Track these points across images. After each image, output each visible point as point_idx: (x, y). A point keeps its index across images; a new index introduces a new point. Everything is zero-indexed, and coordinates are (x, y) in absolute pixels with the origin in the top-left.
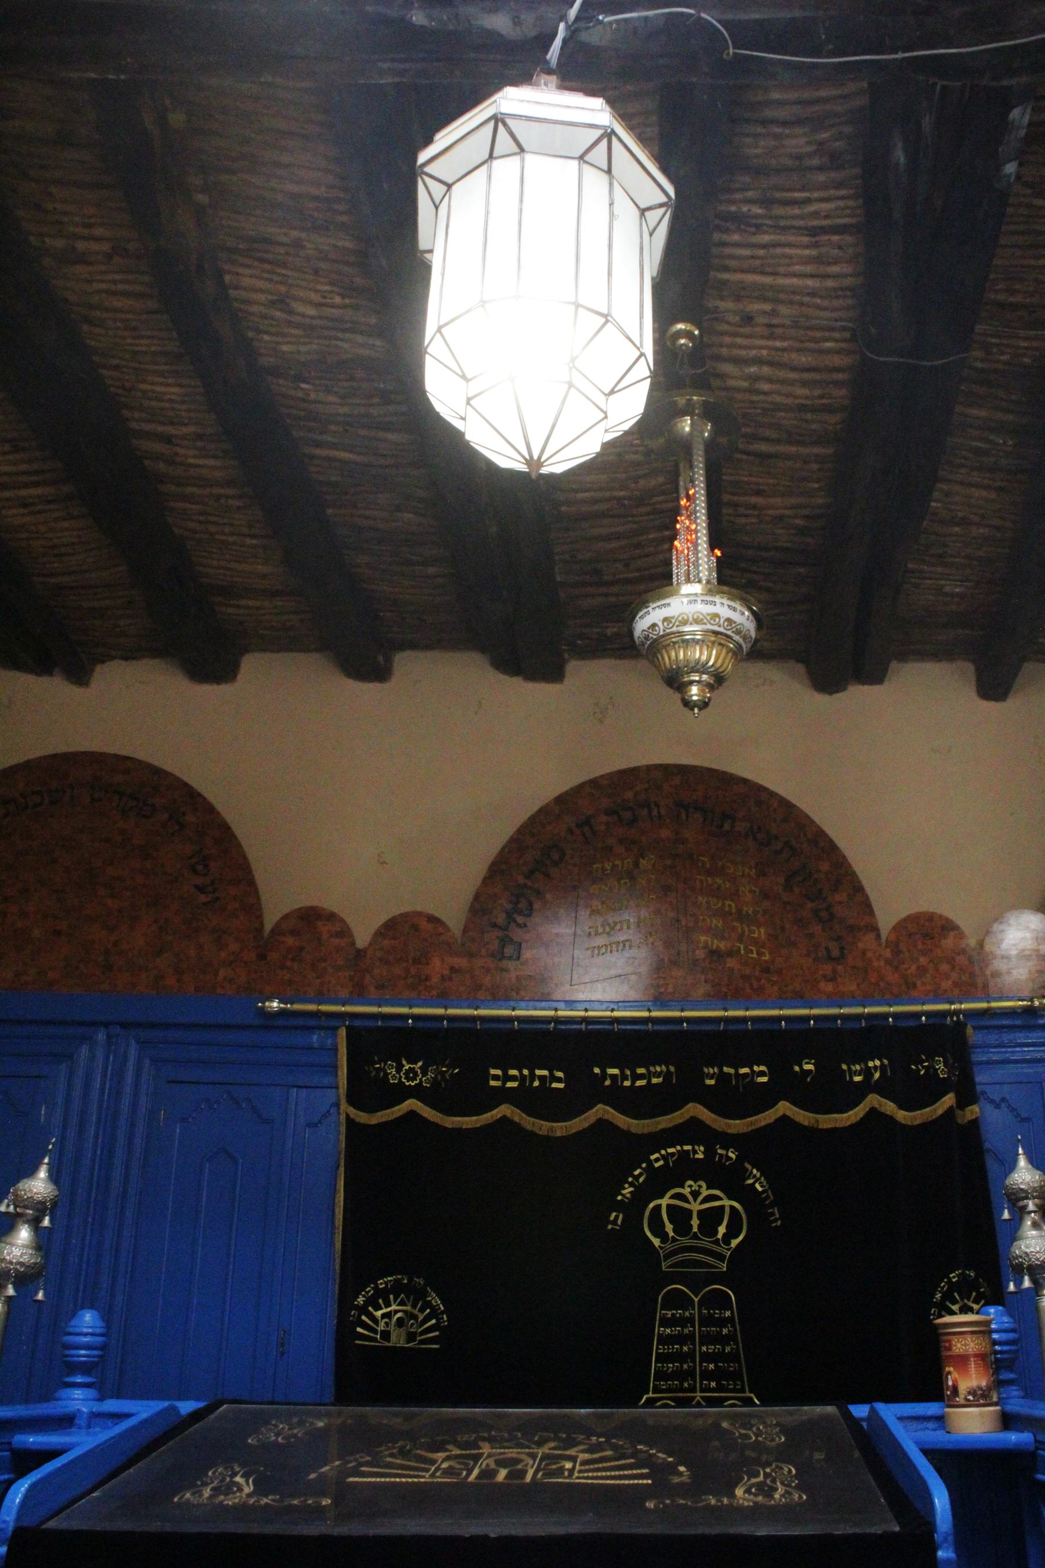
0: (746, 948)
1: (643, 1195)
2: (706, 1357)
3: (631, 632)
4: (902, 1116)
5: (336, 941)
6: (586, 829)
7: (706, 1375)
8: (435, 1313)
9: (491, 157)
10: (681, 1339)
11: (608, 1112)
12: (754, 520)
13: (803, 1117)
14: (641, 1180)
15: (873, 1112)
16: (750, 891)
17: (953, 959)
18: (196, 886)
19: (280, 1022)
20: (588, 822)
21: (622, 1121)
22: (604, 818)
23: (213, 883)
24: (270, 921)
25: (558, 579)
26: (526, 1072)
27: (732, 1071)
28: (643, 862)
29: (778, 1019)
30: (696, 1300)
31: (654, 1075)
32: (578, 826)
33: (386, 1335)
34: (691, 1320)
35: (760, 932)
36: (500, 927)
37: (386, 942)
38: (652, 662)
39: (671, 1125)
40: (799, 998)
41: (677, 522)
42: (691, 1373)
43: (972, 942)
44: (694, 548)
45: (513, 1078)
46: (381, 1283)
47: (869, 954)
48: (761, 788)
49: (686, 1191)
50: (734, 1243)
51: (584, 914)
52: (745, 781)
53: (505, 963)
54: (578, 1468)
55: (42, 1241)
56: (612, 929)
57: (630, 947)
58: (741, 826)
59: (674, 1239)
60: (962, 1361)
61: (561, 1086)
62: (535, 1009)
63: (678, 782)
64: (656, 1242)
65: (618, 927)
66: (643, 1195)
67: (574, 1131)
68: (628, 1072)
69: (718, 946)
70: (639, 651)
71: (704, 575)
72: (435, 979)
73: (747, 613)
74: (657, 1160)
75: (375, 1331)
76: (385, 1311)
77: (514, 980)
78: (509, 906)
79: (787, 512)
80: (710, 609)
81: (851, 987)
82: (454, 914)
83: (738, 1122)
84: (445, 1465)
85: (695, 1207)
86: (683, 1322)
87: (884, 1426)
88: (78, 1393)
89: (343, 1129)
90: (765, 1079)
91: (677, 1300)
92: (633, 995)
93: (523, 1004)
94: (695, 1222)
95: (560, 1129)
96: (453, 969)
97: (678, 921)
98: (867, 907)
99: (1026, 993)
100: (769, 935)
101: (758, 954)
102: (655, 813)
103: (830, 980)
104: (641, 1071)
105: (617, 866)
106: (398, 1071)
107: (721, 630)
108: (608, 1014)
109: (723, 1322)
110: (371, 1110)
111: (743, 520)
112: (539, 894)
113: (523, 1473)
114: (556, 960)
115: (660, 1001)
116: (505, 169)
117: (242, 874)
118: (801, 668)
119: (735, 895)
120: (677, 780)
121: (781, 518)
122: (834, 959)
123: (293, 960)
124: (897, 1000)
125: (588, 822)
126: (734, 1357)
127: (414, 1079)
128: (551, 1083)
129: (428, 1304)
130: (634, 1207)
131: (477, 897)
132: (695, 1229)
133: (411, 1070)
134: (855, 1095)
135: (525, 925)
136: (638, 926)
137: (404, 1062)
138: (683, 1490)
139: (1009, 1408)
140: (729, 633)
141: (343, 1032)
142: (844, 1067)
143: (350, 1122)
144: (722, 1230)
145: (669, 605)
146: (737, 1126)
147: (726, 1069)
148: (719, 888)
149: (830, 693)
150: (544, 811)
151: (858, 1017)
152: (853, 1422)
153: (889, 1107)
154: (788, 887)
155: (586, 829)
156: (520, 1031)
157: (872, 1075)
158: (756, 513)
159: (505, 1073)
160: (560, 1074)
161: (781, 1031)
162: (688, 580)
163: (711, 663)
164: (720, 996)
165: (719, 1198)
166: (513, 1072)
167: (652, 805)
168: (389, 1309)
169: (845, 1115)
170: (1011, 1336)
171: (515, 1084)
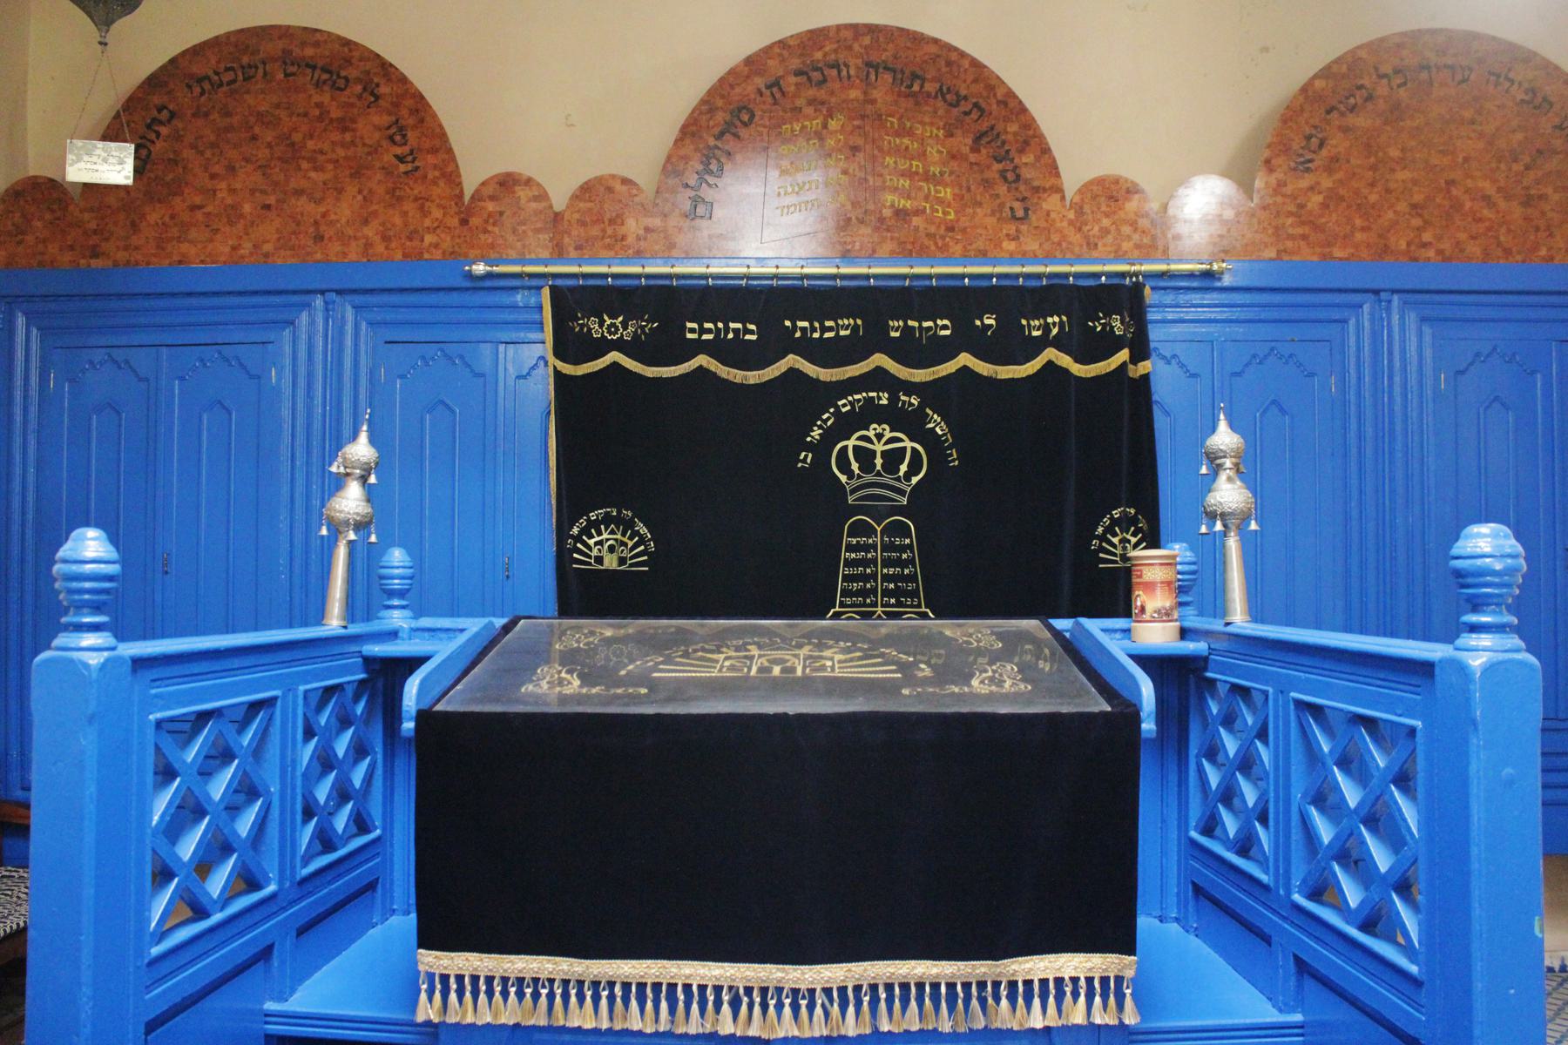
1: (831, 437)
2: (886, 578)
4: (1078, 369)
5: (534, 205)
6: (775, 90)
7: (886, 593)
8: (642, 541)
10: (865, 563)
13: (983, 368)
15: (1050, 363)
17: (1136, 222)
18: (396, 156)
19: (488, 284)
20: (776, 84)
22: (793, 79)
23: (412, 152)
24: (469, 188)
26: (720, 325)
27: (916, 324)
31: (844, 327)
33: (599, 560)
34: (874, 547)
37: (582, 205)
42: (874, 591)
43: (1154, 206)
45: (709, 331)
47: (1053, 215)
48: (951, 48)
49: (871, 434)
50: (915, 480)
51: (774, 174)
52: (936, 41)
54: (836, 662)
55: (370, 494)
58: (930, 87)
59: (859, 477)
60: (1150, 587)
61: (754, 337)
64: (843, 478)
66: (831, 437)
68: (817, 325)
72: (630, 240)
76: (597, 539)
78: (701, 167)
81: (1032, 245)
82: (645, 173)
84: (727, 663)
85: (879, 448)
86: (867, 548)
87: (1090, 636)
88: (396, 613)
89: (552, 380)
90: (948, 332)
91: (861, 529)
92: (821, 251)
94: (879, 461)
95: (753, 377)
96: (647, 230)
97: (866, 180)
98: (1054, 170)
99: (1205, 257)
102: (844, 73)
104: (828, 323)
106: (601, 326)
109: (903, 549)
110: (576, 362)
113: (793, 670)
115: (846, 256)
117: (439, 143)
119: (922, 155)
120: (867, 40)
123: (494, 224)
124: (1080, 259)
126: (912, 578)
129: (637, 533)
130: (822, 449)
132: (879, 467)
133: (613, 325)
134: (1032, 348)
138: (925, 681)
139: (1187, 624)
141: (546, 292)
143: (557, 373)
144: (903, 468)
147: (910, 323)
152: (1057, 634)
153: (1065, 361)
154: (975, 150)
155: (775, 90)
159: (701, 326)
160: (753, 327)
164: (908, 251)
165: (901, 440)
166: (708, 325)
170: (1193, 567)
171: (710, 337)
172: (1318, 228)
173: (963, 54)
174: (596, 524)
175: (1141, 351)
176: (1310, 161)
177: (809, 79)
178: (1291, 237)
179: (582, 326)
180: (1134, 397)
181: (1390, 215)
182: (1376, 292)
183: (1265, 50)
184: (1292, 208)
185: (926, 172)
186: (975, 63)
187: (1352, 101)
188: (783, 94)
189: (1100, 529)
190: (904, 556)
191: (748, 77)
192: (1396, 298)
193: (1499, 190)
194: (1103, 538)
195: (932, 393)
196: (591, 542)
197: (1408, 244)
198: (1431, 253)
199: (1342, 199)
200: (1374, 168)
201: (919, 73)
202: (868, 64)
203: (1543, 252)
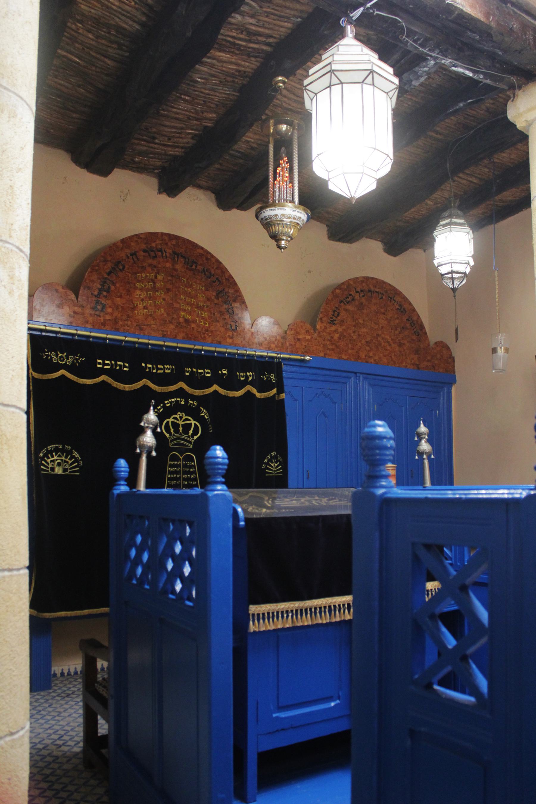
0: (199, 320)
2: (185, 479)
4: (258, 395)
6: (134, 257)
9: (363, 82)
14: (161, 410)
15: (249, 392)
20: (134, 254)
22: (142, 253)
26: (113, 362)
30: (181, 458)
33: (53, 469)
34: (179, 465)
45: (108, 365)
46: (49, 448)
49: (178, 416)
50: (196, 437)
61: (127, 369)
64: (167, 435)
68: (155, 367)
74: (168, 403)
75: (48, 468)
85: (181, 423)
90: (209, 375)
91: (175, 458)
92: (66, 323)
94: (181, 429)
95: (127, 387)
102: (164, 255)
104: (160, 366)
106: (57, 356)
109: (191, 467)
116: (336, 89)
118: (213, 196)
119: (196, 297)
120: (174, 242)
127: (63, 361)
129: (74, 457)
132: (181, 431)
133: (62, 357)
137: (59, 353)
142: (238, 373)
144: (191, 432)
146: (198, 393)
148: (190, 293)
149: (224, 210)
153: (254, 391)
154: (217, 297)
155: (134, 257)
156: (93, 342)
159: (104, 362)
160: (127, 365)
165: (190, 420)
168: (53, 459)
171: (109, 367)
172: (337, 347)
173: (212, 256)
174: (51, 452)
175: (281, 390)
176: (335, 320)
177: (149, 255)
178: (329, 349)
179: (48, 356)
180: (276, 408)
181: (360, 344)
182: (356, 373)
183: (309, 272)
184: (329, 338)
185: (198, 304)
186: (217, 261)
187: (348, 299)
188: (138, 259)
189: (266, 460)
190: (192, 470)
191: (122, 248)
192: (361, 375)
193: (392, 339)
194: (267, 464)
195: (203, 400)
196: (49, 461)
197: (366, 356)
198: (372, 360)
199: (344, 336)
200: (355, 326)
201: (195, 261)
202: (175, 253)
203: (404, 364)
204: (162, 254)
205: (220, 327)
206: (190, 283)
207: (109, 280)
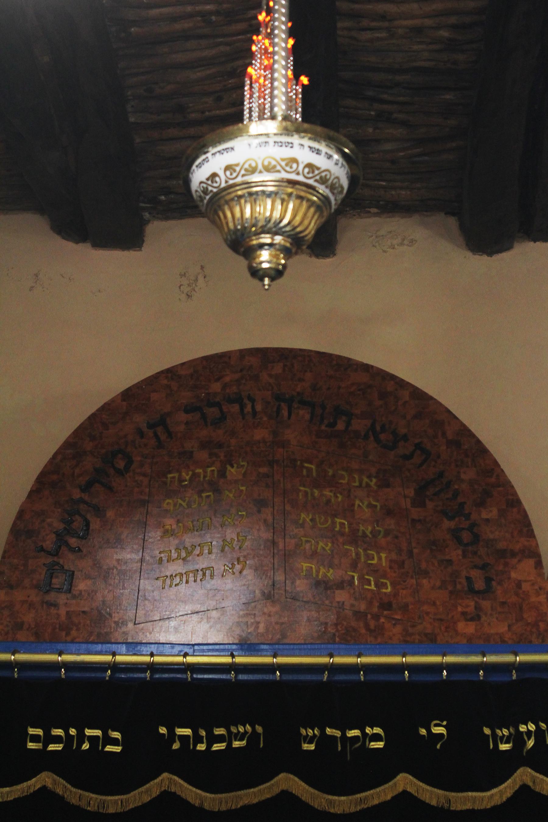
0: (361, 578)
3: (187, 182)
6: (160, 430)
11: (176, 783)
12: (383, 35)
13: (431, 795)
16: (370, 506)
20: (162, 422)
21: (192, 793)
22: (183, 417)
25: (132, 120)
26: (73, 732)
27: (338, 733)
28: (232, 471)
29: (399, 668)
31: (233, 738)
32: (151, 426)
35: (380, 558)
36: (49, 553)
38: (213, 222)
39: (255, 801)
40: (431, 643)
41: (253, 42)
44: (273, 73)
45: (57, 740)
47: (525, 586)
52: (367, 368)
53: (52, 597)
56: (189, 553)
57: (212, 576)
58: (359, 425)
61: (118, 749)
62: (89, 653)
63: (280, 371)
65: (197, 551)
67: (132, 806)
68: (203, 733)
69: (325, 575)
70: (197, 207)
71: (280, 109)
73: (336, 157)
77: (63, 618)
79: (428, 22)
80: (287, 153)
83: (343, 798)
90: (380, 745)
93: (73, 647)
95: (114, 803)
97: (274, 543)
100: (391, 561)
101: (376, 585)
102: (249, 408)
103: (472, 619)
104: (219, 731)
105: (198, 475)
107: (300, 178)
108: (180, 659)
111: (368, 35)
112: (99, 511)
114: (119, 591)
118: (452, 222)
119: (348, 511)
120: (278, 369)
121: (418, 30)
122: (478, 592)
125: (162, 422)
128: (104, 746)
131: (21, 514)
135: (80, 550)
136: (223, 551)
140: (311, 182)
142: (487, 731)
145: (232, 149)
147: (329, 731)
148: (328, 501)
149: (490, 254)
150: (106, 408)
151: (507, 668)
154: (419, 501)
155: (160, 430)
157: (524, 743)
158: (386, 24)
159: (47, 733)
160: (116, 735)
161: (403, 683)
162: (261, 117)
163: (285, 221)
164: (328, 641)
167: (246, 401)
169: (488, 794)
171: (58, 747)
177: (204, 417)
186: (157, 373)
202: (279, 398)
204: (242, 407)
205: (433, 588)
206: (331, 472)
207: (85, 503)
